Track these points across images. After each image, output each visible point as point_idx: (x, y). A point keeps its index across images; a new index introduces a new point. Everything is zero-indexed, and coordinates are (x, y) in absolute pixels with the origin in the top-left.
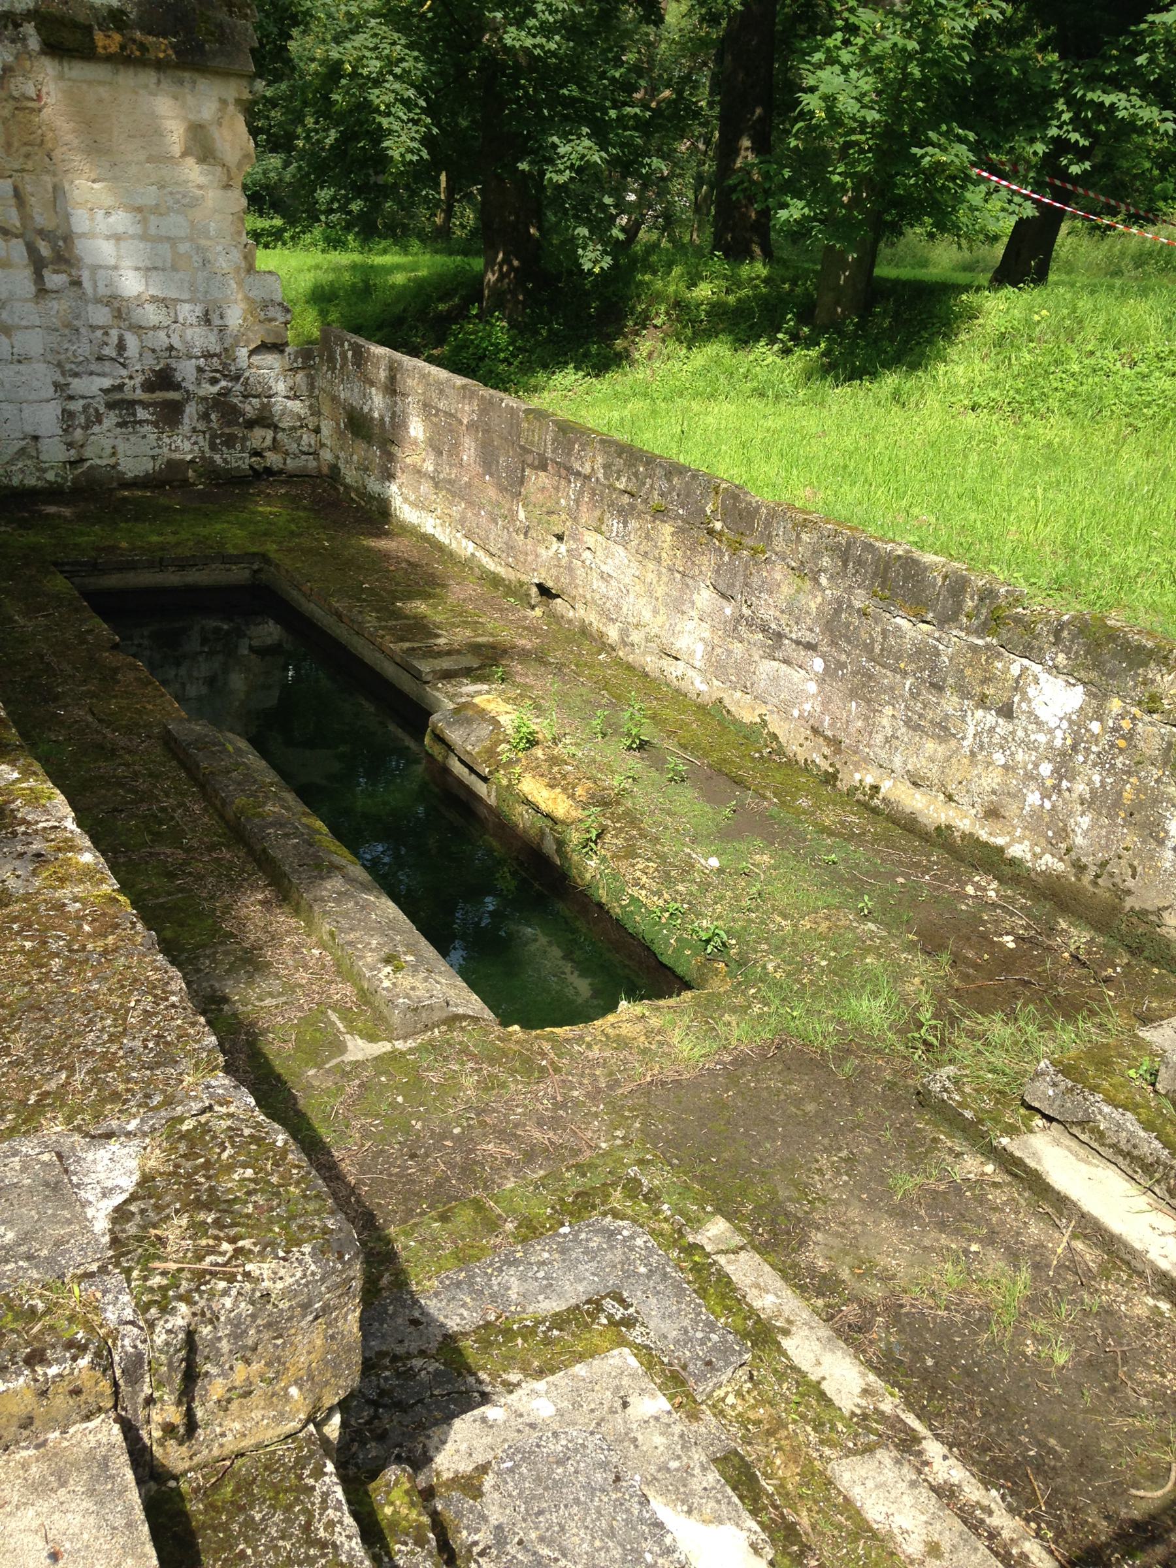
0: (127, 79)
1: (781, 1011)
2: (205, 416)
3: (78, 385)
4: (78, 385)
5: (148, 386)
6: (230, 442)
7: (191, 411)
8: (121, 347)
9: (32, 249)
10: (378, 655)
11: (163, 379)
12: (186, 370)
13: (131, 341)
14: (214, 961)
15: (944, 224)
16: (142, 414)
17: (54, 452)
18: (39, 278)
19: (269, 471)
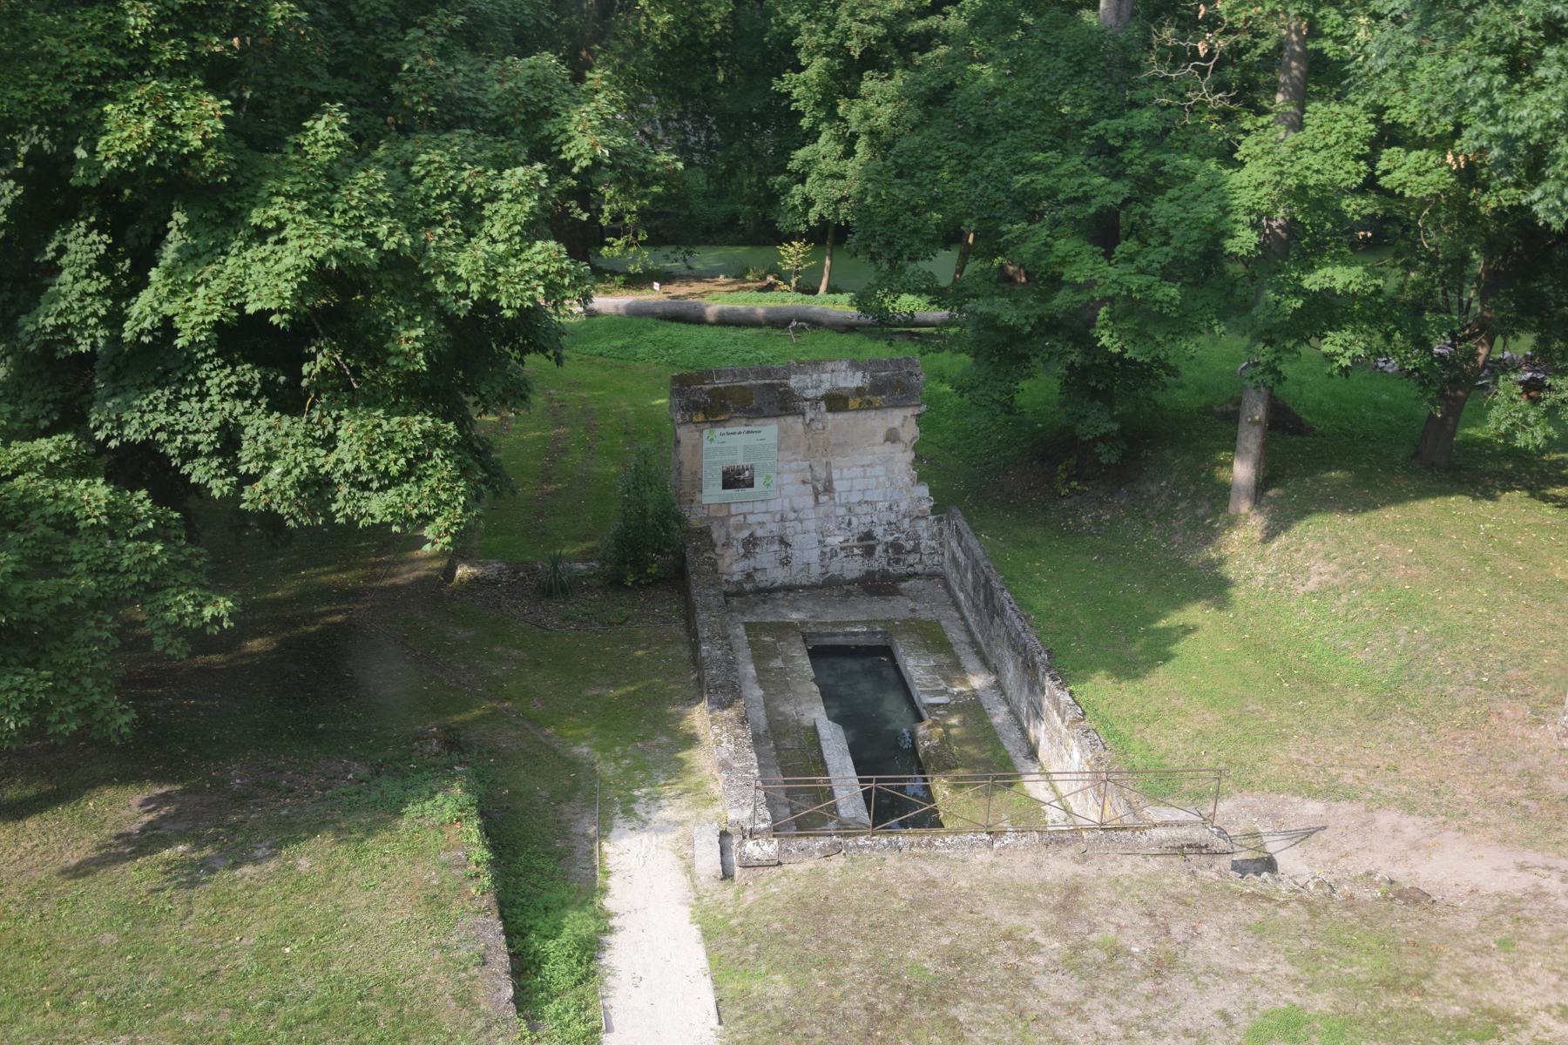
0: (862, 415)
1: (1108, 381)
2: (886, 551)
3: (829, 540)
4: (829, 540)
5: (860, 539)
6: (897, 561)
7: (879, 549)
8: (850, 523)
9: (814, 488)
10: (967, 614)
11: (868, 536)
12: (879, 531)
13: (854, 520)
14: (870, 1008)
15: (1233, 237)
16: (856, 551)
17: (816, 570)
18: (816, 499)
19: (916, 574)
